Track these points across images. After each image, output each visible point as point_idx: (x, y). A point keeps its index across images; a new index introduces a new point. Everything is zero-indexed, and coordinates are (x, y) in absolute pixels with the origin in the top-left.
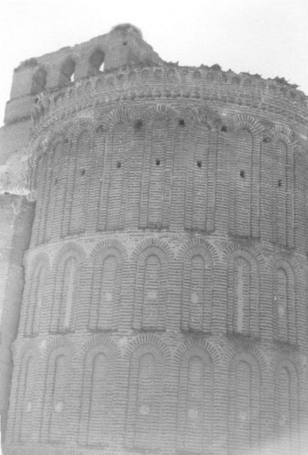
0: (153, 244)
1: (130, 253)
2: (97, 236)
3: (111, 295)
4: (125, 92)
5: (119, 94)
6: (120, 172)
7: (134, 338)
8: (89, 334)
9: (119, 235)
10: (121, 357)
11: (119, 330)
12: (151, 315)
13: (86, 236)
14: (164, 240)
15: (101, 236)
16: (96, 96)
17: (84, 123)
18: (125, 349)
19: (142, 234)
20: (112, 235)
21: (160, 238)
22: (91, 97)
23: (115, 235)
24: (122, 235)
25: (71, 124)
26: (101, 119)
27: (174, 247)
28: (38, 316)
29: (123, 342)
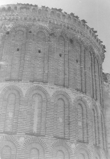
0: (81, 99)
1: (73, 100)
2: (55, 87)
3: (62, 119)
4: (65, 24)
5: (61, 23)
6: (61, 59)
7: (78, 145)
8: (54, 138)
9: (66, 90)
10: (72, 154)
11: (71, 139)
12: (80, 134)
13: (48, 85)
14: (85, 99)
15: (58, 88)
16: (50, 18)
17: (41, 28)
18: (74, 150)
19: (76, 92)
20: (63, 89)
21: (84, 97)
22: (47, 18)
23: (64, 89)
24: (68, 90)
25: (33, 25)
26: (53, 30)
27: (88, 103)
28: (93, 130)
29: (22, 140)
